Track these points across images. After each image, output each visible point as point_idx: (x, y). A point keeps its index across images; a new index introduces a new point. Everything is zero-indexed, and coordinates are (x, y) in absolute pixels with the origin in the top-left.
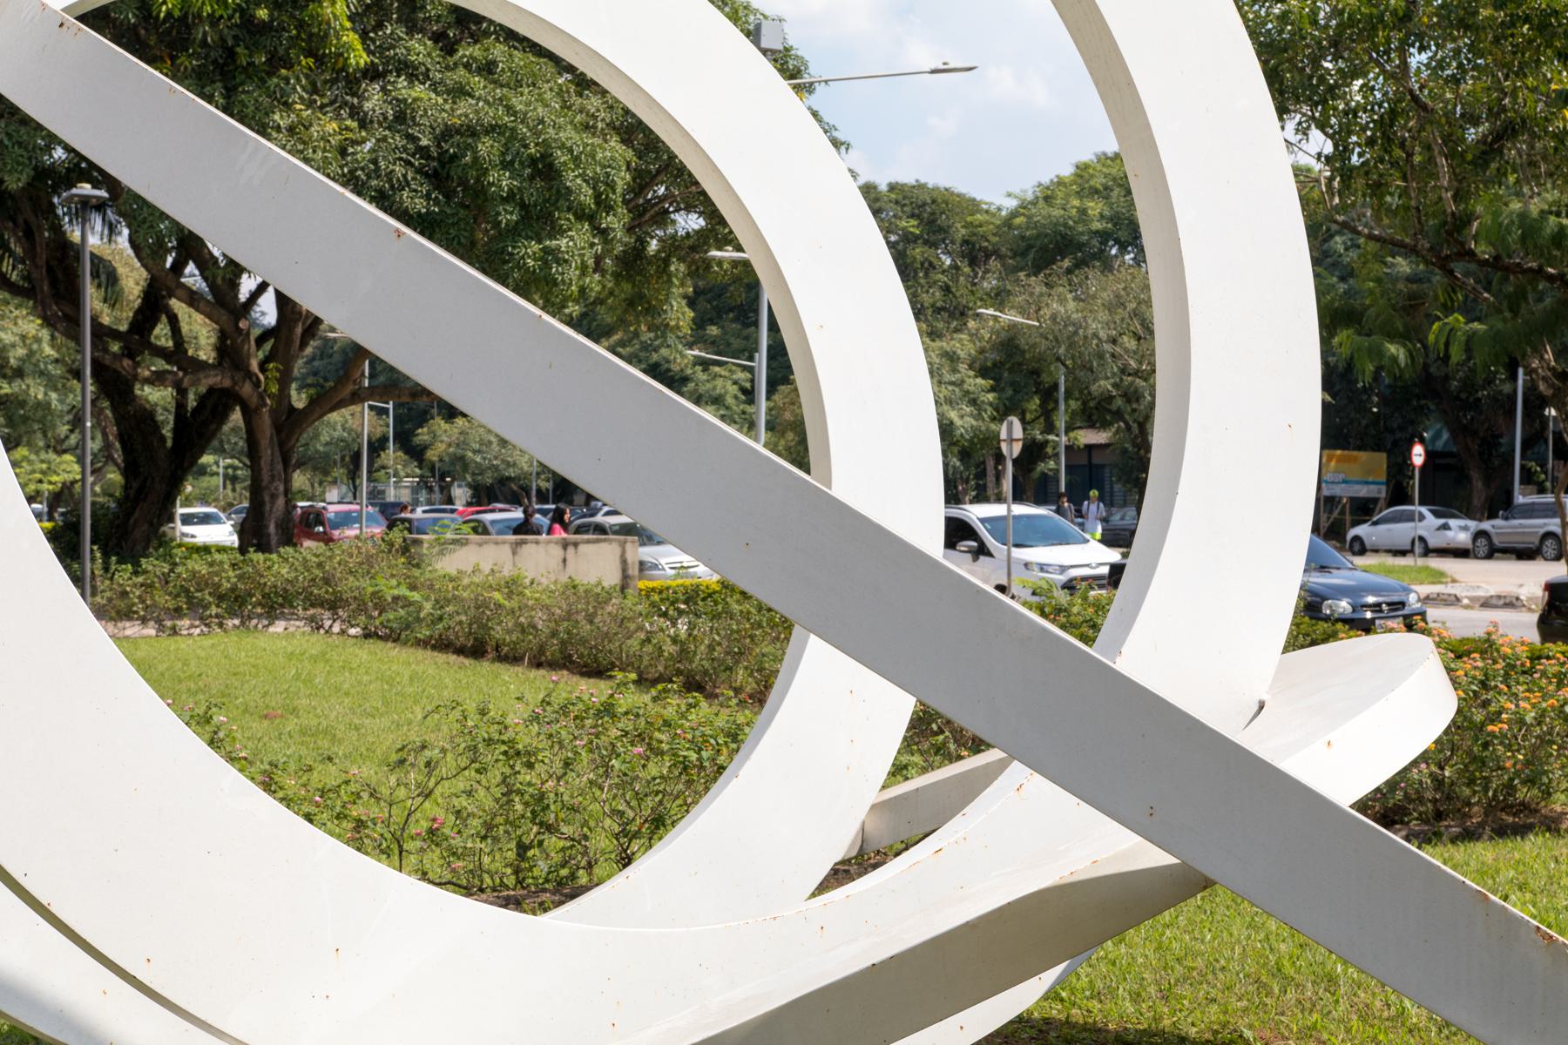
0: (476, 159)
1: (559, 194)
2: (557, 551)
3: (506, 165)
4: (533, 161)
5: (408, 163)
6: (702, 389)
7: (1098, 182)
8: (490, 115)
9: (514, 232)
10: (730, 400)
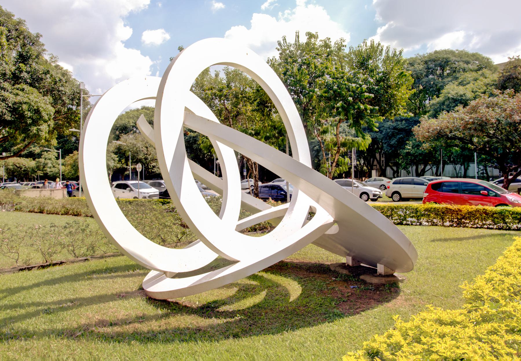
0: (22, 109)
1: (41, 117)
2: (49, 192)
3: (29, 111)
4: (35, 110)
5: (7, 109)
6: (46, 157)
7: (131, 116)
8: (26, 100)
9: (30, 125)
10: (53, 159)
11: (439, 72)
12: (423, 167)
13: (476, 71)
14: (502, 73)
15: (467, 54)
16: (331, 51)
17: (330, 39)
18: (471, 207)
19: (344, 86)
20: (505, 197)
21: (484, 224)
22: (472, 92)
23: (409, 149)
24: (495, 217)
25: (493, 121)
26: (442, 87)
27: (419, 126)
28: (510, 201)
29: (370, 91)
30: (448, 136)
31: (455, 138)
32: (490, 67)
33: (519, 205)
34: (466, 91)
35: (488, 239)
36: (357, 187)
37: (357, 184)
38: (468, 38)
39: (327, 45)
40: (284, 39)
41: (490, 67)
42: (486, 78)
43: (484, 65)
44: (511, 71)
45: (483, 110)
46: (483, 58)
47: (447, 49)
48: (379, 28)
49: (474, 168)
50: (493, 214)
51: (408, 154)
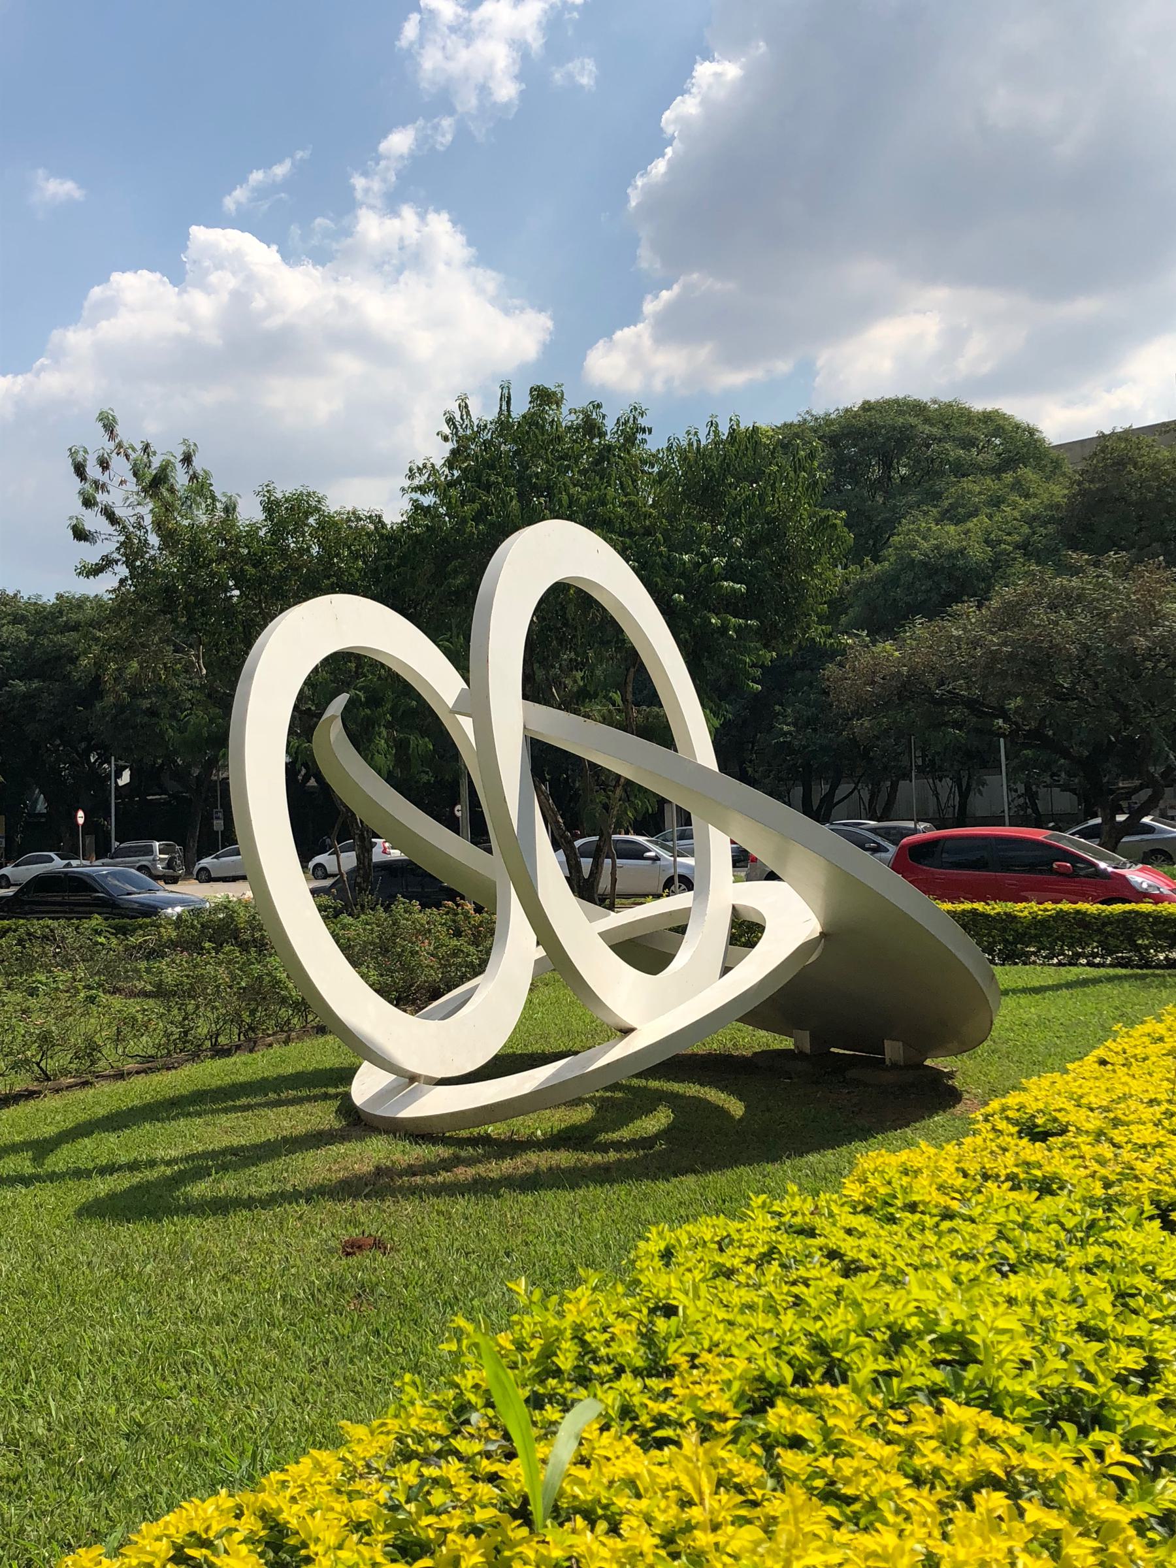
11: (876, 472)
12: (825, 788)
13: (997, 471)
14: (1079, 483)
15: (967, 417)
16: (609, 448)
17: (599, 406)
18: (1042, 907)
19: (658, 560)
20: (1123, 877)
21: (1079, 955)
22: (986, 542)
23: (785, 734)
24: (1109, 934)
25: (1073, 649)
26: (891, 524)
27: (841, 665)
28: (1137, 886)
29: (732, 573)
30: (932, 695)
31: (954, 699)
32: (1038, 459)
33: (1171, 901)
34: (966, 539)
35: (1107, 988)
36: (656, 859)
37: (654, 850)
38: (955, 338)
39: (591, 427)
40: (464, 408)
41: (1038, 459)
42: (1027, 496)
43: (1018, 448)
44: (1109, 477)
45: (1040, 615)
46: (1017, 427)
47: (901, 396)
48: (649, 297)
49: (998, 789)
50: (1104, 924)
51: (786, 748)
